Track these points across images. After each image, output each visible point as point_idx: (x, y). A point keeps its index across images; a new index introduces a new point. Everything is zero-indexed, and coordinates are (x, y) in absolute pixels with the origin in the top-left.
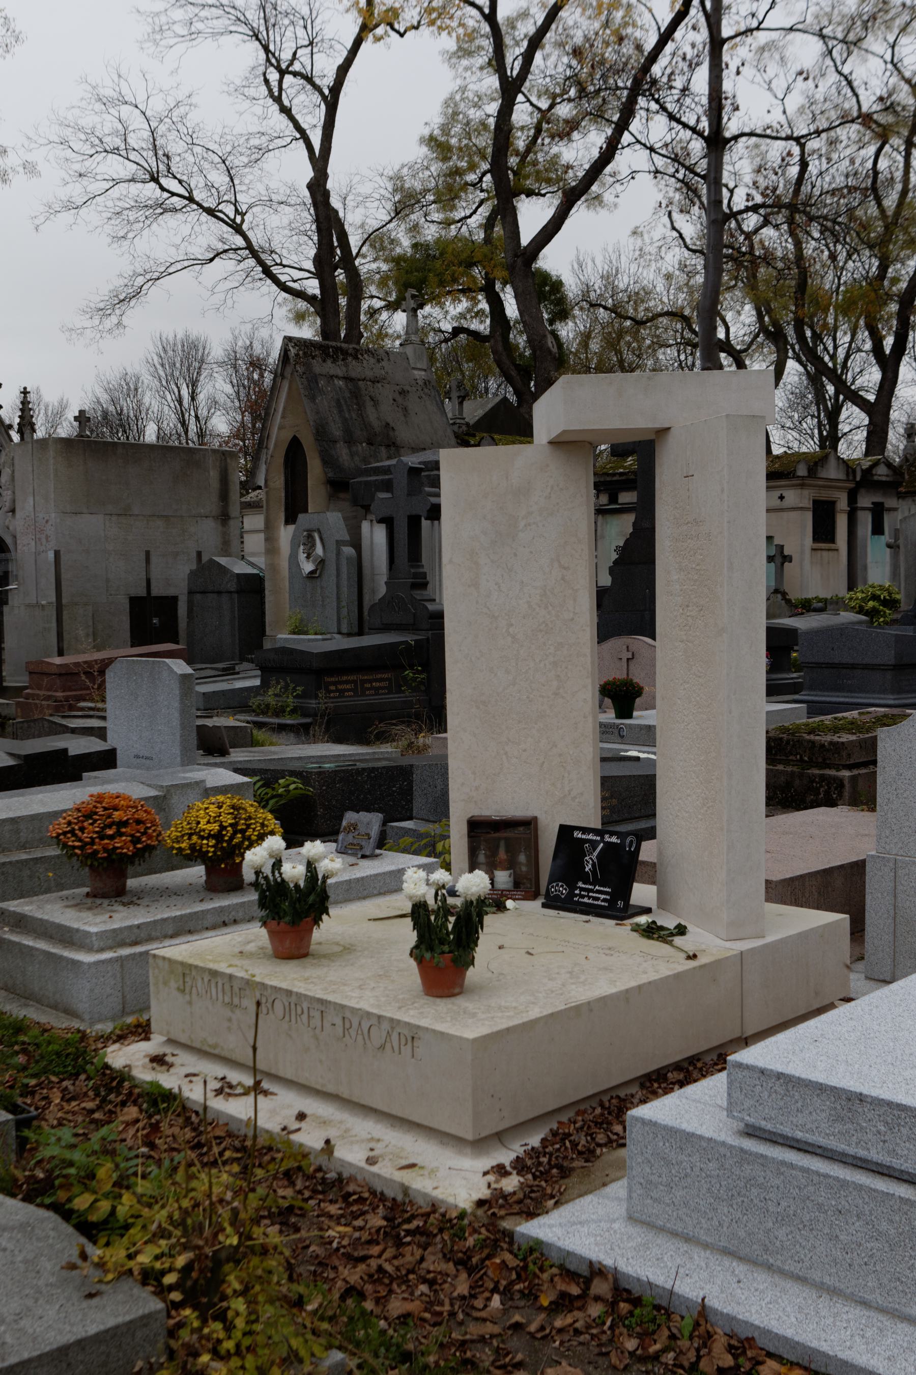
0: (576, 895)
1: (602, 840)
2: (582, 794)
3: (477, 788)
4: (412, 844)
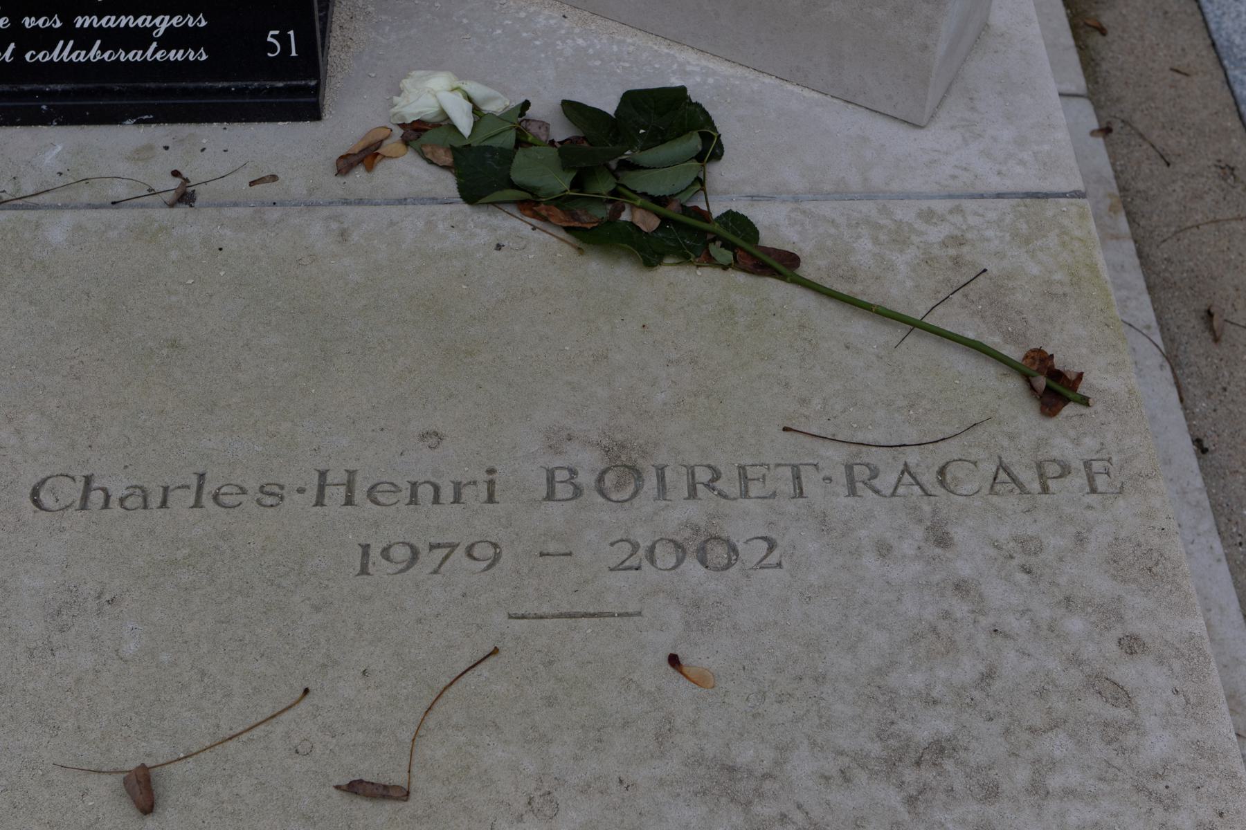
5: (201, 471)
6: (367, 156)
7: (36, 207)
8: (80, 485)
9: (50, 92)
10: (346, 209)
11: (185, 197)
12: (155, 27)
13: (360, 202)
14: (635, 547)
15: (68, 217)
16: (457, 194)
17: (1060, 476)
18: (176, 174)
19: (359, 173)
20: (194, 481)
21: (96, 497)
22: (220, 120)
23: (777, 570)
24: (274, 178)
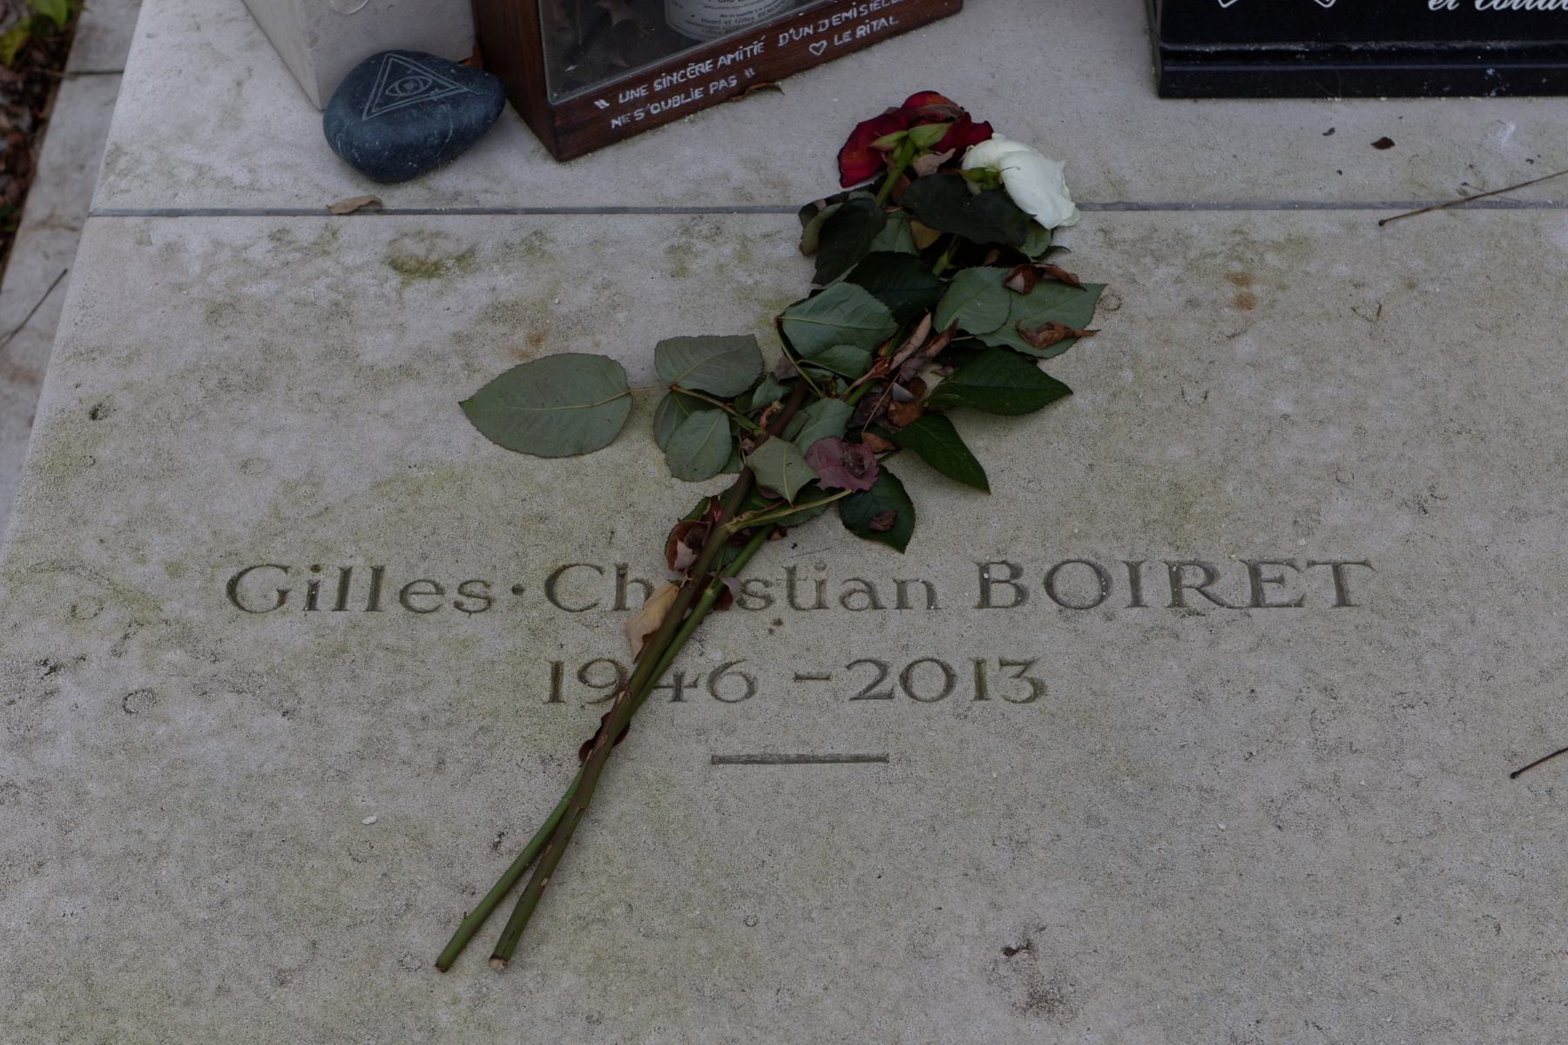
7: (1518, 205)
9: (1493, 50)
14: (884, 669)
17: (1016, 603)
23: (887, 701)
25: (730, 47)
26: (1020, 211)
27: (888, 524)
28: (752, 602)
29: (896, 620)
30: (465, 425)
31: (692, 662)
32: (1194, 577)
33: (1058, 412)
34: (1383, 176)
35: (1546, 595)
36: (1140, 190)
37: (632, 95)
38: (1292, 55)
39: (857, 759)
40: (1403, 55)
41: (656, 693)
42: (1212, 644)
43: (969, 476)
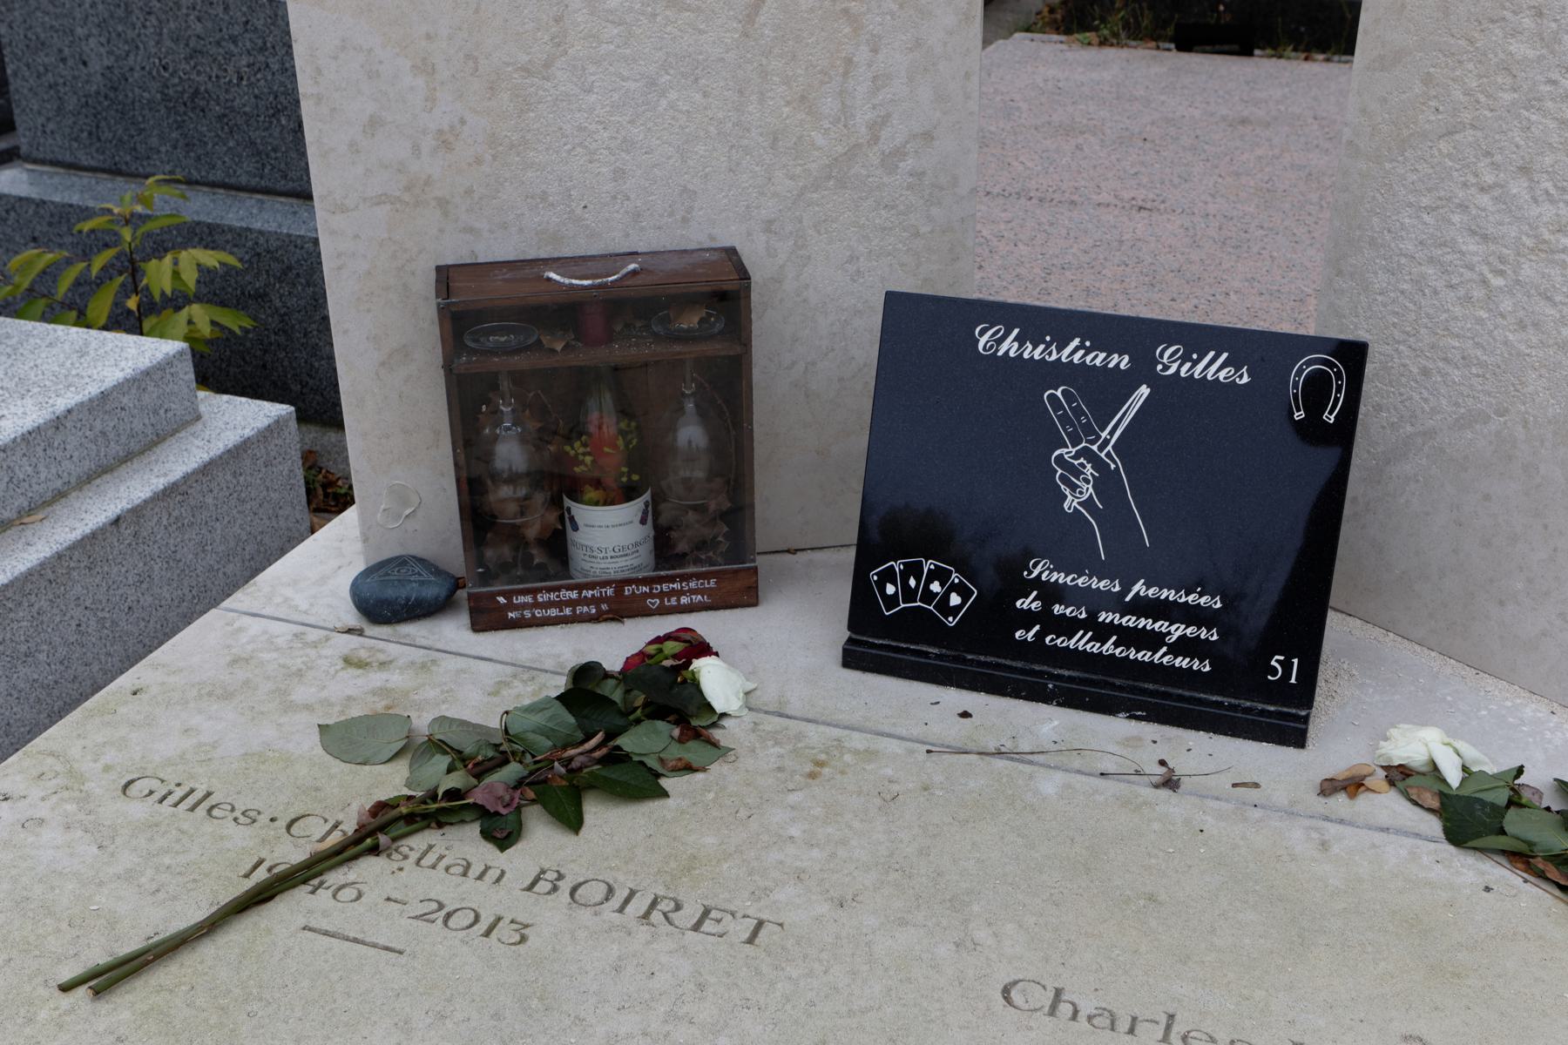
0: (1027, 619)
1: (1144, 369)
2: (928, 136)
3: (445, 142)
4: (50, 274)
5: (1171, 1011)
6: (1353, 785)
7: (1031, 763)
8: (1051, 994)
10: (1328, 825)
11: (1170, 782)
12: (1169, 633)
13: (1342, 822)
15: (1059, 776)
16: (1442, 835)
18: (1162, 763)
19: (1341, 798)
20: (1163, 1020)
21: (1065, 1009)
22: (1207, 730)
24: (1256, 785)
25: (591, 586)
26: (701, 692)
27: (502, 834)
28: (395, 856)
29: (470, 883)
30: (316, 737)
31: (334, 878)
32: (666, 906)
33: (654, 805)
34: (957, 731)
35: (886, 970)
36: (795, 707)
37: (522, 599)
38: (926, 654)
39: (387, 949)
40: (998, 666)
41: (303, 887)
42: (648, 943)
43: (574, 823)
